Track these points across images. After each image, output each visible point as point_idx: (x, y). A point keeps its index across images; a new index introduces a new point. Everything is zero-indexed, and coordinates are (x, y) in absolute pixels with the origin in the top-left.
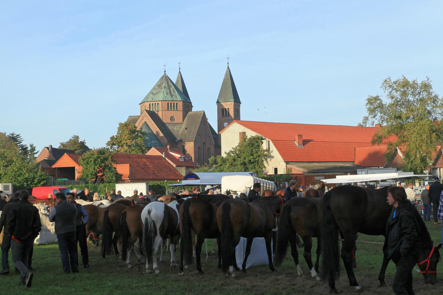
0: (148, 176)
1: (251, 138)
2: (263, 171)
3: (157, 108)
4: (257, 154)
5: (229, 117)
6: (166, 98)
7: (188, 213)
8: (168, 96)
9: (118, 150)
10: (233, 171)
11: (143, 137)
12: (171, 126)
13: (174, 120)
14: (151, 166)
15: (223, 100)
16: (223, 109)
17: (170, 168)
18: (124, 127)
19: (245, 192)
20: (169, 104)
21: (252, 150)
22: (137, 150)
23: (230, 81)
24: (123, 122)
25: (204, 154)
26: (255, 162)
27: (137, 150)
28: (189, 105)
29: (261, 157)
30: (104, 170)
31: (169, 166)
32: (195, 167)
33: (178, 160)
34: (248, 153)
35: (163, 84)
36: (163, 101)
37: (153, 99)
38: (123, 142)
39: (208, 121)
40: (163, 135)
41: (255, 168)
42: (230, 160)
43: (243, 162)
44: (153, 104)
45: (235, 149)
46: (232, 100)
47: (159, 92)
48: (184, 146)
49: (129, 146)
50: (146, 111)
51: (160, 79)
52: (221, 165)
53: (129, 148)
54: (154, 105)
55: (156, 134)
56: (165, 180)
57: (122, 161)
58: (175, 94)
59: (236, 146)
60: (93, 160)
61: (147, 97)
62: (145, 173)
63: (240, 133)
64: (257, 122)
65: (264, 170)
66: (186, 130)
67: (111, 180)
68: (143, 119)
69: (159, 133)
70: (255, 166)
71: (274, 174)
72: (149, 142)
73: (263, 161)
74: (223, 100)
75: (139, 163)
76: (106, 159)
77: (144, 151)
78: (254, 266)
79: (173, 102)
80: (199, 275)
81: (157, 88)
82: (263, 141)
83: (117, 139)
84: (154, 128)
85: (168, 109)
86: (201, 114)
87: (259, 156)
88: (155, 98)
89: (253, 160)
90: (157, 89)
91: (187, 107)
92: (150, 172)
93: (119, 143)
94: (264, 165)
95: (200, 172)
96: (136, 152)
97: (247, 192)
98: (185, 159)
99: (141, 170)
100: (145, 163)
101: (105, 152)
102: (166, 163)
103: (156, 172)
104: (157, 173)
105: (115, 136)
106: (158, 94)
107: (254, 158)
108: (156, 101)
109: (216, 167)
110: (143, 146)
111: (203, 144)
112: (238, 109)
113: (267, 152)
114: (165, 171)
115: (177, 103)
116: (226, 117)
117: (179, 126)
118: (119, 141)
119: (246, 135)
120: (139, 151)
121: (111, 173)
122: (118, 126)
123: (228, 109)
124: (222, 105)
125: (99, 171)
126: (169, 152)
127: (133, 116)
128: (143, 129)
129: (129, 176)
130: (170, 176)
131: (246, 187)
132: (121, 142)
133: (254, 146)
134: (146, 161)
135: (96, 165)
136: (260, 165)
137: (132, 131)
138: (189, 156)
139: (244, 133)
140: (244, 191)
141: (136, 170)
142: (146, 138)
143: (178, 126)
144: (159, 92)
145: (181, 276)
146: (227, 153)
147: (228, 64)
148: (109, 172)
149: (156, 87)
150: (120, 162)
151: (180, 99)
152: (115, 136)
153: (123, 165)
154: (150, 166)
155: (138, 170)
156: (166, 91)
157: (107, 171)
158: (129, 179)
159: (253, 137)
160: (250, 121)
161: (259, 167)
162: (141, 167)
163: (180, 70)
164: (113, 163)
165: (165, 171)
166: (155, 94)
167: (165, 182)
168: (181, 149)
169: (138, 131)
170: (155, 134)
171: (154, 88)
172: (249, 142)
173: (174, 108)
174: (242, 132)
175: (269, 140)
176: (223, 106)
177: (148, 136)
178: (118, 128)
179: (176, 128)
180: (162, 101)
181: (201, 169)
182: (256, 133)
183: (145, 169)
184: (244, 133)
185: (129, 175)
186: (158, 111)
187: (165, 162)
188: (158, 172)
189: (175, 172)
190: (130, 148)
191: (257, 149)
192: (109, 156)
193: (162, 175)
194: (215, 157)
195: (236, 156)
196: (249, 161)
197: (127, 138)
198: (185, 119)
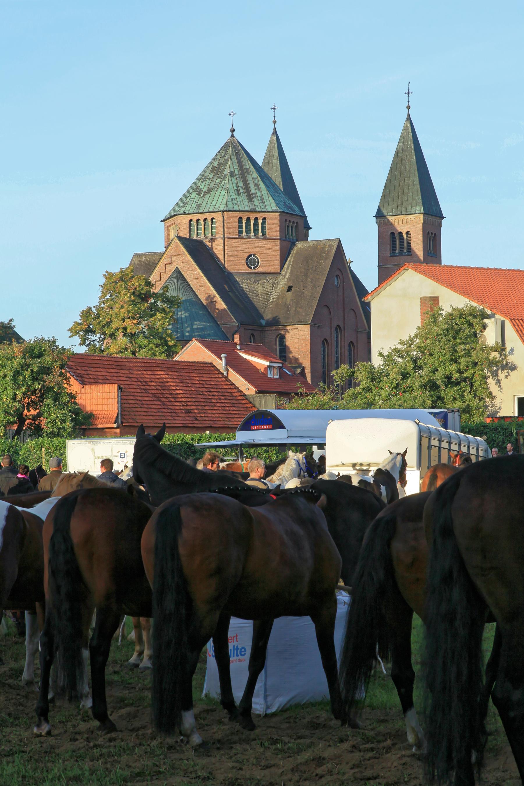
0: (170, 418)
1: (451, 315)
2: (486, 407)
3: (210, 231)
4: (468, 359)
5: (409, 257)
6: (236, 204)
7: (67, 539)
8: (239, 199)
9: (101, 346)
10: (400, 406)
11: (171, 311)
12: (249, 281)
13: (257, 265)
14: (181, 392)
15: (394, 210)
16: (393, 234)
17: (233, 396)
18: (117, 283)
19: (388, 468)
20: (244, 221)
21: (454, 347)
22: (154, 348)
23: (414, 157)
24: (115, 270)
25: (337, 358)
26: (465, 380)
27: (154, 348)
28: (297, 223)
29: (479, 367)
30: (42, 402)
31: (230, 391)
32: (293, 394)
33: (263, 374)
34: (444, 355)
35: (225, 164)
36: (226, 211)
37: (199, 206)
38: (115, 325)
39: (353, 267)
40: (226, 304)
41: (463, 396)
42: (392, 376)
43: (430, 381)
44: (198, 220)
45: (409, 343)
46: (418, 208)
47: (214, 188)
48: (282, 338)
49: (133, 336)
50: (180, 239)
51: (219, 152)
52: (368, 389)
53: (131, 342)
54: (203, 223)
55: (207, 304)
56: (204, 429)
57: (100, 377)
58: (259, 194)
59: (412, 336)
60: (10, 373)
61: (183, 202)
62: (164, 410)
63: (423, 300)
64: (472, 268)
65: (488, 403)
66: (290, 294)
67: (59, 429)
68: (171, 263)
69: (215, 299)
70: (464, 391)
71: (516, 415)
72: (186, 325)
73: (485, 378)
74: (394, 210)
75: (146, 382)
76: (46, 370)
77: (173, 349)
78: (298, 706)
79: (253, 216)
80: (99, 733)
81: (211, 176)
82: (486, 321)
83: (98, 316)
84: (200, 286)
85: (239, 236)
86: (331, 249)
87: (475, 364)
88: (205, 202)
89: (458, 374)
90: (209, 179)
91: (292, 227)
92: (177, 408)
93: (103, 326)
94: (488, 388)
95: (306, 408)
96: (151, 352)
97: (395, 464)
98: (282, 373)
99: (152, 403)
100: (163, 385)
101: (45, 350)
102: (222, 383)
103: (194, 407)
104: (196, 411)
105: (94, 307)
106: (213, 193)
107: (459, 371)
108: (207, 211)
109: (353, 394)
110: (170, 335)
111: (337, 332)
112: (435, 234)
113: (498, 353)
114: (218, 405)
115: (264, 219)
116: (402, 257)
117: (271, 281)
118: (104, 323)
119: (441, 304)
120: (157, 349)
121: (61, 409)
122: (103, 281)
123: (408, 233)
124: (391, 224)
125: (28, 404)
126: (239, 353)
127: (146, 255)
128: (171, 288)
129: (117, 417)
130: (233, 418)
131: (391, 453)
132: (109, 324)
133: (461, 336)
134: (167, 376)
135: (18, 388)
136: (476, 390)
137: (141, 294)
138: (298, 363)
139: (435, 300)
140: (386, 462)
141: (138, 402)
142: (179, 313)
143: (267, 280)
144: (214, 188)
145: (40, 736)
146: (383, 357)
147: (409, 107)
148: (56, 405)
149: (206, 175)
150: (92, 381)
151: (274, 207)
152: (93, 309)
153: (101, 386)
154: (177, 390)
155: (144, 402)
156: (234, 185)
157: (48, 405)
158: (115, 425)
159: (459, 310)
160: (452, 267)
161: (475, 396)
162: (152, 393)
163: (275, 128)
164: (65, 382)
165: (218, 405)
166: (206, 193)
167: (204, 435)
168: (276, 346)
169: (156, 294)
170: (205, 304)
171: (202, 178)
172: (446, 325)
173: (256, 233)
174: (429, 295)
175: (503, 319)
176: (394, 228)
177: (185, 310)
178: (101, 286)
179: (263, 287)
180: (223, 211)
181: (308, 400)
182: (468, 300)
183: (164, 399)
184: (435, 300)
185: (115, 416)
186: (211, 239)
187: (220, 380)
188: (199, 407)
189: (247, 407)
190: (135, 340)
191: (468, 343)
192: (56, 361)
193: (210, 415)
194: (351, 367)
195: (411, 365)
196: (446, 378)
197: (125, 313)
198: (288, 262)
